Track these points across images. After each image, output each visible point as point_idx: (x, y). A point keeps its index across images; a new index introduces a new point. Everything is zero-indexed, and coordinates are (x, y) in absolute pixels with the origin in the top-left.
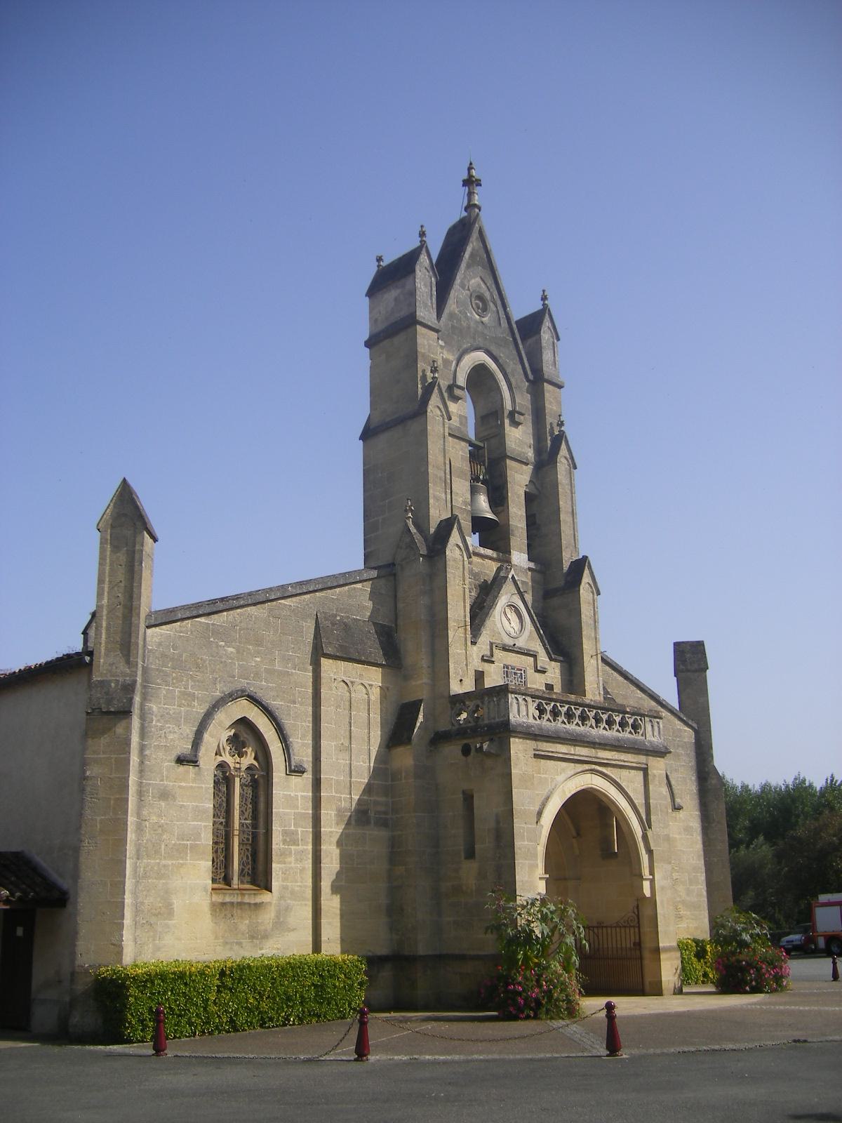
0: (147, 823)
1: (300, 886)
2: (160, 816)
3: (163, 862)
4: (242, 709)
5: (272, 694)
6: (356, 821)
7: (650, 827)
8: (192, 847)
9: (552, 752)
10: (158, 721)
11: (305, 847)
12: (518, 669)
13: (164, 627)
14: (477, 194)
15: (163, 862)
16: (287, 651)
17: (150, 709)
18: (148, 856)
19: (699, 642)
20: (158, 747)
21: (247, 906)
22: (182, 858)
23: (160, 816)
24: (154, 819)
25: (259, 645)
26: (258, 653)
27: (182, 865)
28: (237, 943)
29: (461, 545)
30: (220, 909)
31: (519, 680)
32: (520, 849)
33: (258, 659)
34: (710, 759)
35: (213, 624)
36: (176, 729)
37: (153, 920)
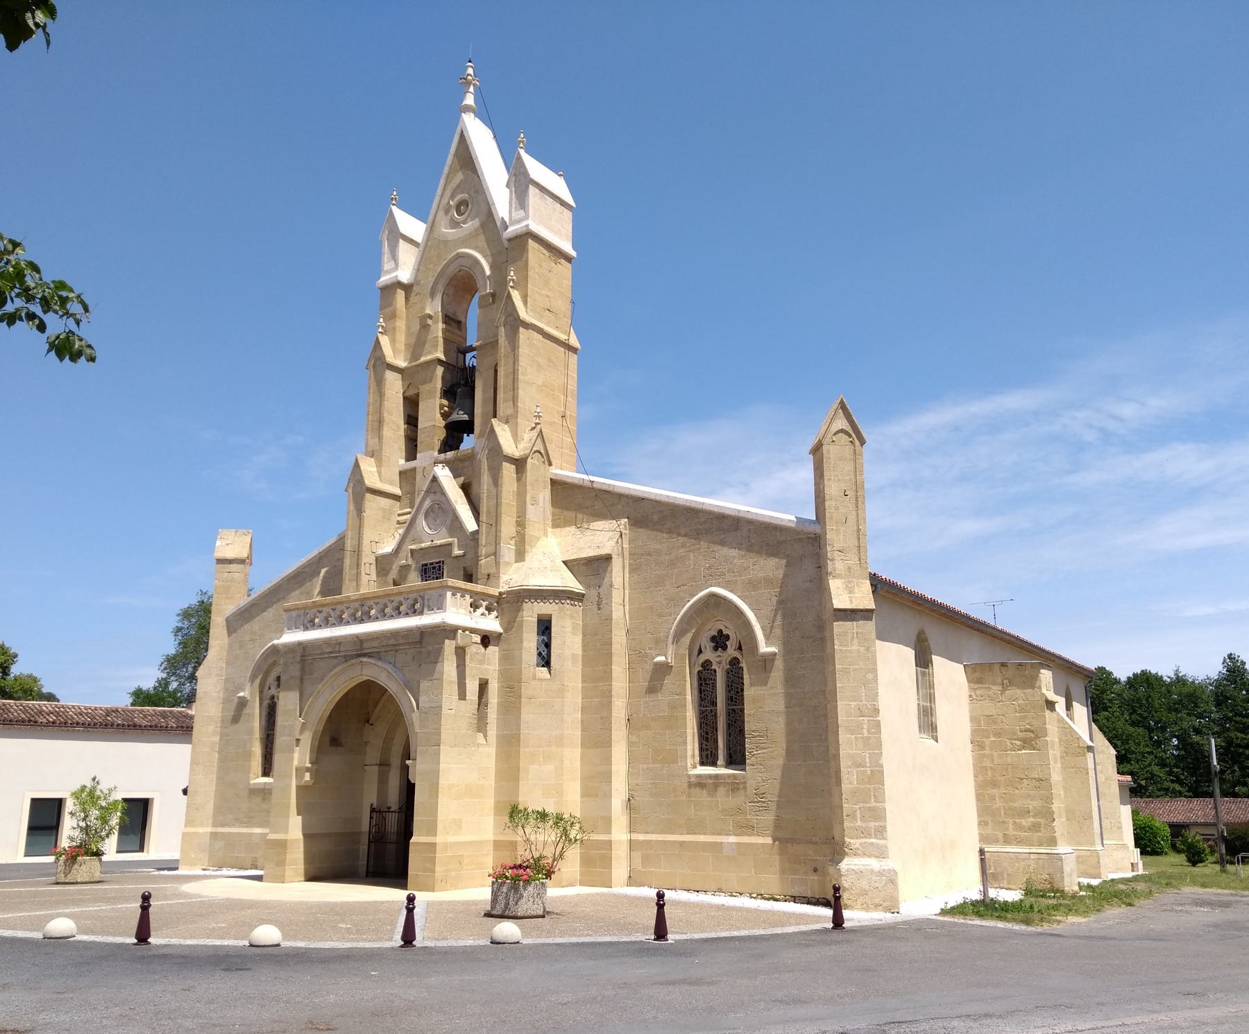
12: (437, 563)
29: (542, 451)
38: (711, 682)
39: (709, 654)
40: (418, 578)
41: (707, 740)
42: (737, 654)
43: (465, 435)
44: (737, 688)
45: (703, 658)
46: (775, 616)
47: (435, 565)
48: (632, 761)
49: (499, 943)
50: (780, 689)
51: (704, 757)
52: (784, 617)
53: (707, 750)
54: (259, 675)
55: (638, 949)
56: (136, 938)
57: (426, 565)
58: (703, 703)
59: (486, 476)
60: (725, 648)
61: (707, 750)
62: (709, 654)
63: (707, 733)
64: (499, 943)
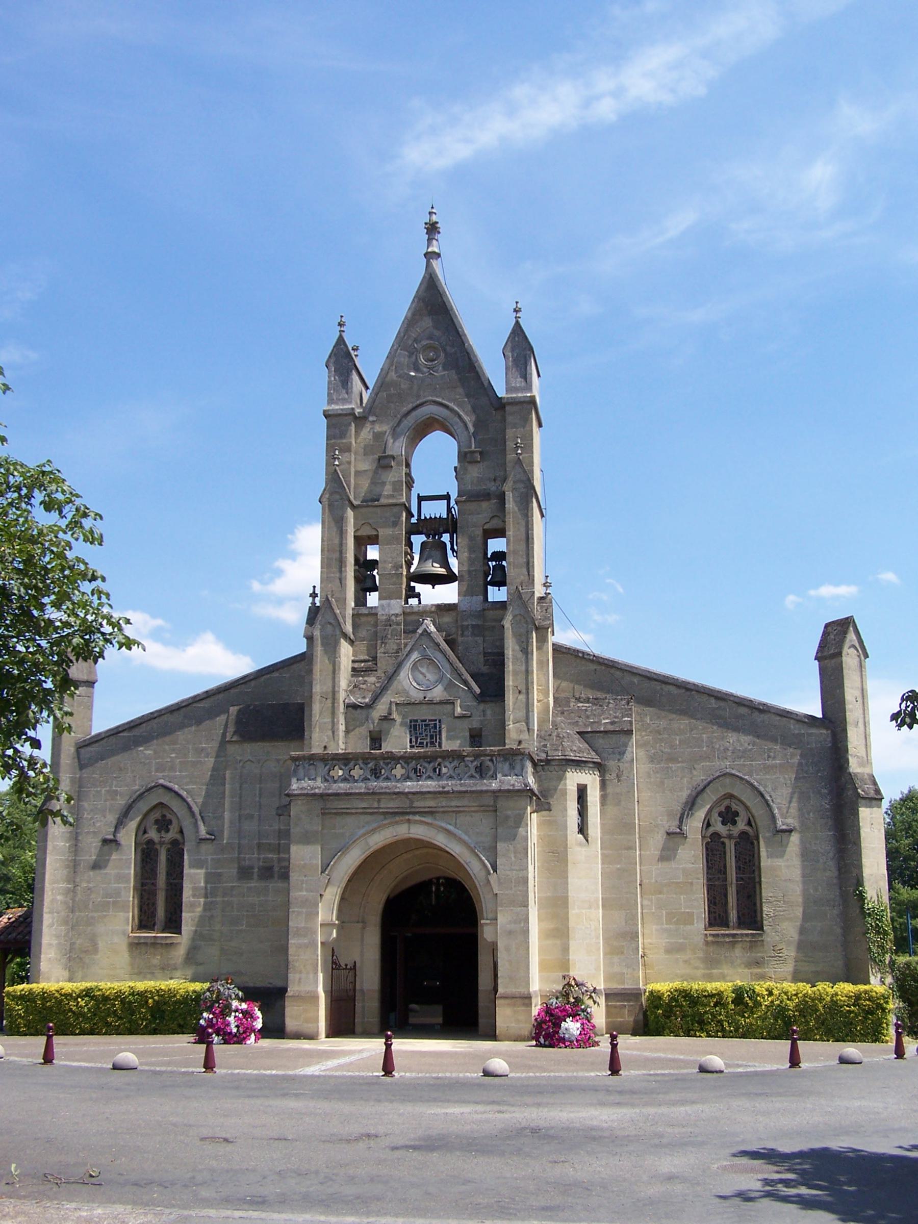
0: (79, 888)
1: (209, 930)
2: (89, 882)
3: (91, 914)
4: (153, 799)
5: (185, 781)
6: (258, 876)
7: (495, 871)
8: (114, 903)
9: (347, 809)
10: (88, 814)
11: (214, 899)
12: (430, 720)
13: (94, 745)
14: (437, 240)
15: (91, 914)
16: (201, 743)
17: (82, 806)
18: (80, 911)
19: (847, 618)
20: (88, 833)
21: (159, 946)
22: (105, 911)
23: (89, 882)
24: (84, 885)
25: (173, 744)
26: (173, 750)
27: (105, 916)
28: (150, 973)
29: (332, 621)
30: (135, 945)
31: (432, 730)
32: (296, 899)
33: (173, 755)
34: (846, 765)
35: (134, 736)
36: (102, 818)
37: (82, 956)
38: (718, 853)
39: (153, 834)
40: (406, 733)
41: (715, 904)
42: (178, 837)
43: (368, 593)
44: (745, 859)
45: (711, 830)
46: (791, 798)
47: (427, 722)
48: (540, 920)
49: (497, 1076)
50: (796, 862)
51: (712, 919)
52: (800, 800)
53: (715, 912)
54: (137, 817)
55: (370, 1083)
56: (610, 1070)
57: (416, 721)
58: (710, 871)
59: (510, 641)
60: (734, 823)
61: (715, 912)
62: (153, 834)
63: (715, 898)
64: (497, 1076)
